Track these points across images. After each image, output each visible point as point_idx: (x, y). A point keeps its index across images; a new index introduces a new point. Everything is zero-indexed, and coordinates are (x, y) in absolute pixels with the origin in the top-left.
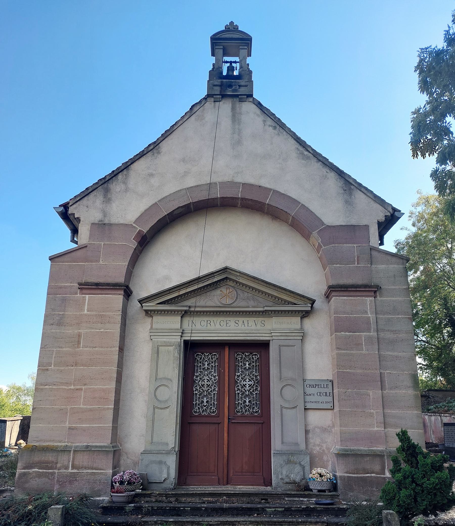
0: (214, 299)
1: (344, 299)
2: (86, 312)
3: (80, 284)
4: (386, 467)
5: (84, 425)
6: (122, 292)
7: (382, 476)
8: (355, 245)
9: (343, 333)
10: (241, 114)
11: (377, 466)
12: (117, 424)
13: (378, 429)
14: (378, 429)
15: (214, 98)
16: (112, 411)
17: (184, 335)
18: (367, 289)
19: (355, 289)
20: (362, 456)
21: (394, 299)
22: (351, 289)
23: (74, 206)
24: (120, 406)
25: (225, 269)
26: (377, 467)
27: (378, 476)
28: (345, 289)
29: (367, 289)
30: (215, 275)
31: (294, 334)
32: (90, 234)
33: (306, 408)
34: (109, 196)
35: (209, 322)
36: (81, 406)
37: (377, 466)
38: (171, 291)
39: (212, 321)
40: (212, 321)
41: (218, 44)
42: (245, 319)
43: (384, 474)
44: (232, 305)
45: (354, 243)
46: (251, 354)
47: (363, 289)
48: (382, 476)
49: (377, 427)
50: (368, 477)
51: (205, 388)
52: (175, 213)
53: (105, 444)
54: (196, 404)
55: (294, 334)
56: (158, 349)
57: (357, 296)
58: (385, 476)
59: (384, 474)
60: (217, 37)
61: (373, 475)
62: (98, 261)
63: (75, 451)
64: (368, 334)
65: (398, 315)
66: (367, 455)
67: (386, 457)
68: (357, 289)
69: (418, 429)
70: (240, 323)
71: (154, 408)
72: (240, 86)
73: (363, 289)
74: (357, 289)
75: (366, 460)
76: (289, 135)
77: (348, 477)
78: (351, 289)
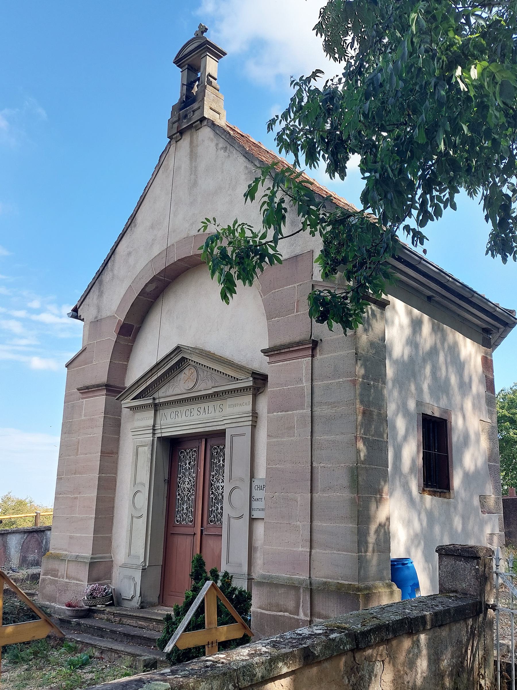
0: (181, 385)
1: (280, 365)
2: (83, 418)
3: (79, 389)
4: (301, 605)
5: (78, 535)
6: (105, 392)
7: (296, 617)
8: (296, 285)
9: (275, 414)
10: (197, 146)
11: (292, 602)
12: (111, 533)
13: (302, 549)
14: (302, 549)
15: (174, 138)
16: (93, 521)
17: (156, 432)
18: (301, 347)
19: (288, 350)
20: (277, 586)
21: (335, 354)
22: (284, 351)
23: (81, 307)
24: (115, 514)
25: (178, 349)
26: (291, 604)
27: (292, 616)
28: (278, 352)
29: (301, 347)
30: (171, 356)
31: (243, 419)
32: (89, 334)
33: (253, 517)
34: (102, 289)
35: (177, 413)
36: (77, 515)
37: (292, 602)
38: (139, 384)
39: (179, 412)
40: (179, 412)
41: (183, 65)
42: (206, 405)
43: (298, 615)
44: (193, 390)
45: (295, 282)
46: (191, 450)
47: (297, 348)
48: (296, 617)
49: (302, 547)
50: (280, 616)
51: (186, 493)
52: (148, 290)
53: (87, 555)
54: (212, 510)
55: (243, 419)
56: (137, 450)
57: (95, 396)
58: (298, 617)
59: (298, 615)
60: (180, 57)
61: (287, 614)
62: (92, 362)
63: (68, 561)
64: (301, 411)
65: (339, 377)
66: (282, 586)
67: (301, 591)
68: (291, 349)
69: (351, 551)
70: (211, 409)
71: (132, 517)
72: (194, 111)
73: (297, 348)
74: (291, 349)
75: (280, 592)
76: (238, 153)
77: (261, 613)
78: (284, 351)
